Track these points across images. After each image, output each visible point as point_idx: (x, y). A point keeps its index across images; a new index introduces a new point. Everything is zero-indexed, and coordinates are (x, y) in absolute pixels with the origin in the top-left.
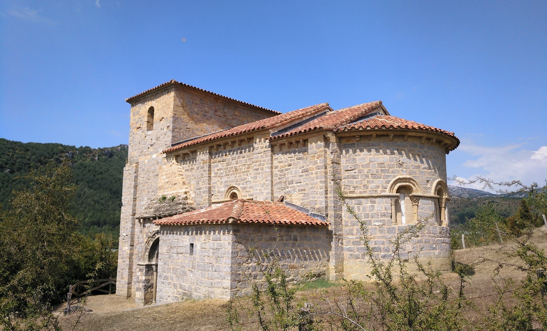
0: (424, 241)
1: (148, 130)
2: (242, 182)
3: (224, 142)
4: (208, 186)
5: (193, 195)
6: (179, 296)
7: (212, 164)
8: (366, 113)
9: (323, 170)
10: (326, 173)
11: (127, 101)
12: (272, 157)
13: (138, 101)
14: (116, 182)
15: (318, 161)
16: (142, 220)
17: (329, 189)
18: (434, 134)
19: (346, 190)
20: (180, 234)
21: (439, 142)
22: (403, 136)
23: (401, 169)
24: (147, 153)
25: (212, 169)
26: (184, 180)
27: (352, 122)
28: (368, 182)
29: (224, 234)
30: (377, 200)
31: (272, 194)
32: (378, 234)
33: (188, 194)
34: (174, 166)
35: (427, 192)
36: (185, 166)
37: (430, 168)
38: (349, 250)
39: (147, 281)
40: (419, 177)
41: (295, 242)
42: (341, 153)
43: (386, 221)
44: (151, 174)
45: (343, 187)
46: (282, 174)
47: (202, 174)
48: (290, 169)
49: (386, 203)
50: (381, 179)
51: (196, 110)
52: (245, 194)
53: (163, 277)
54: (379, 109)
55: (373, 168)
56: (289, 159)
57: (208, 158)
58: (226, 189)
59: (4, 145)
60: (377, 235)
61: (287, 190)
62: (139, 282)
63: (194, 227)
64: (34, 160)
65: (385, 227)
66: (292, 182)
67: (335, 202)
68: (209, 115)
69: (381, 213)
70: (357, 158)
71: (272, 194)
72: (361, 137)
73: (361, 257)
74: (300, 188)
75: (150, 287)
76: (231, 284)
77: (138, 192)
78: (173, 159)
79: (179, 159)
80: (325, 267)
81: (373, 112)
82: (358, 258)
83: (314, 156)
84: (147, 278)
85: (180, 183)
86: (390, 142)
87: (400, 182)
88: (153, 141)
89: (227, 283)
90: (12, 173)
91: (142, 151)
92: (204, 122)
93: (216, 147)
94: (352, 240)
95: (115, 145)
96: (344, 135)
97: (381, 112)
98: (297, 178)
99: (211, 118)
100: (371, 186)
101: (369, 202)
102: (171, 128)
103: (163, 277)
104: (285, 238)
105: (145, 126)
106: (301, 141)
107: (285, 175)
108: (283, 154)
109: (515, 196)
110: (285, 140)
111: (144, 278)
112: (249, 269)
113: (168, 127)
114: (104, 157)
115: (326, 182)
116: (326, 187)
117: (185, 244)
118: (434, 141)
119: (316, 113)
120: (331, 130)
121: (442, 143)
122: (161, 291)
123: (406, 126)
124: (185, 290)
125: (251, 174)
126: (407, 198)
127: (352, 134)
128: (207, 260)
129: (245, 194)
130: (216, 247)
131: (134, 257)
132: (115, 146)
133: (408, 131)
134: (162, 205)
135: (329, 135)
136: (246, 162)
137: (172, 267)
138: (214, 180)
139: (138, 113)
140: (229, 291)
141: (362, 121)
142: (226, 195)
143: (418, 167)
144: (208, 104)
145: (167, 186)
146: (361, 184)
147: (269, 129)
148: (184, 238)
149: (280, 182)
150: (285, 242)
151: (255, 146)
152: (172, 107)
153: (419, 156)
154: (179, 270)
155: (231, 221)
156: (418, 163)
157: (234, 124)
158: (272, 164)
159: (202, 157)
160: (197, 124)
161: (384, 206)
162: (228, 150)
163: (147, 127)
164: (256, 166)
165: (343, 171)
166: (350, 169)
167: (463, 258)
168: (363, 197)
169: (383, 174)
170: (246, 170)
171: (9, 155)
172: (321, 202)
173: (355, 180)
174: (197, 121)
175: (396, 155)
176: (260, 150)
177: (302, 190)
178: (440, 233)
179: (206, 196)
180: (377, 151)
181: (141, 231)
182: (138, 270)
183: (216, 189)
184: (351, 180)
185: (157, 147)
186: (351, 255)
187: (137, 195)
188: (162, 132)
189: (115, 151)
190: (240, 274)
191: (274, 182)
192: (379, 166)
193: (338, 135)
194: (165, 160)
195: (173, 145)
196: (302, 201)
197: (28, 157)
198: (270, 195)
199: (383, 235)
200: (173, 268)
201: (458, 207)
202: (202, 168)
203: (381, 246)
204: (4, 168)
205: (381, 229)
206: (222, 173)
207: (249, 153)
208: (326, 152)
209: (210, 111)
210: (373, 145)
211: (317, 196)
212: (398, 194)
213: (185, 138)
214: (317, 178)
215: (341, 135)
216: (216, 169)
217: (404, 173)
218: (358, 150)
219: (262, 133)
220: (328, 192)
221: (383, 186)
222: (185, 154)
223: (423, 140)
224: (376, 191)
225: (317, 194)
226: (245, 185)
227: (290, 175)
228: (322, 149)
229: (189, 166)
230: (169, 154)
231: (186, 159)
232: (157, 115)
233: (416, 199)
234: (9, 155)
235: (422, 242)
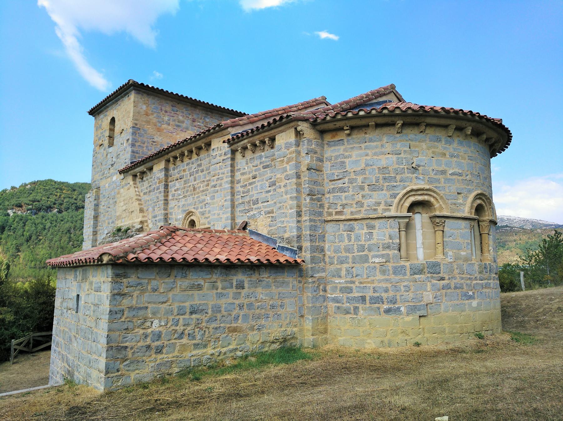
0: (453, 286)
1: (109, 147)
2: (201, 205)
4: (163, 212)
9: (294, 180)
10: (299, 184)
15: (288, 168)
17: (304, 209)
19: (330, 210)
22: (417, 125)
23: (415, 175)
24: (108, 175)
28: (363, 196)
30: (377, 223)
32: (379, 277)
33: (145, 224)
35: (458, 211)
38: (336, 300)
40: (444, 188)
41: (239, 291)
43: (391, 256)
45: (326, 206)
46: (246, 190)
47: (158, 198)
48: (254, 182)
49: (391, 227)
50: (384, 192)
56: (254, 168)
59: (52, 185)
60: (377, 278)
61: (252, 213)
64: (80, 200)
65: (390, 265)
66: (256, 202)
67: (313, 228)
68: (184, 125)
73: (352, 311)
74: (267, 209)
80: (296, 326)
82: (347, 312)
83: (283, 161)
85: (136, 210)
86: (398, 135)
88: (114, 160)
90: (60, 213)
94: (339, 286)
96: (325, 127)
98: (264, 195)
100: (366, 202)
101: (365, 228)
102: (130, 141)
104: (219, 284)
105: (106, 143)
106: (267, 140)
107: (248, 191)
110: (246, 141)
112: (146, 337)
118: (469, 132)
127: (339, 124)
133: (426, 116)
135: (303, 127)
136: (205, 178)
138: (172, 204)
144: (183, 113)
146: (353, 199)
147: (228, 128)
149: (243, 203)
150: (219, 290)
152: (131, 115)
155: (106, 259)
158: (232, 176)
161: (388, 231)
165: (326, 181)
166: (336, 178)
167: (521, 305)
168: (356, 220)
169: (388, 184)
170: (205, 188)
171: (56, 196)
172: (291, 228)
173: (344, 194)
183: (174, 216)
184: (339, 194)
186: (338, 308)
187: (98, 228)
190: (126, 347)
192: (381, 172)
197: (75, 197)
198: (230, 221)
199: (386, 277)
201: (520, 239)
203: (383, 294)
204: (52, 208)
205: (384, 268)
208: (299, 153)
209: (186, 121)
212: (410, 214)
216: (173, 189)
217: (419, 181)
219: (220, 133)
222: (143, 173)
224: (375, 210)
225: (286, 217)
226: (204, 209)
227: (255, 192)
231: (144, 179)
234: (56, 196)
235: (450, 288)
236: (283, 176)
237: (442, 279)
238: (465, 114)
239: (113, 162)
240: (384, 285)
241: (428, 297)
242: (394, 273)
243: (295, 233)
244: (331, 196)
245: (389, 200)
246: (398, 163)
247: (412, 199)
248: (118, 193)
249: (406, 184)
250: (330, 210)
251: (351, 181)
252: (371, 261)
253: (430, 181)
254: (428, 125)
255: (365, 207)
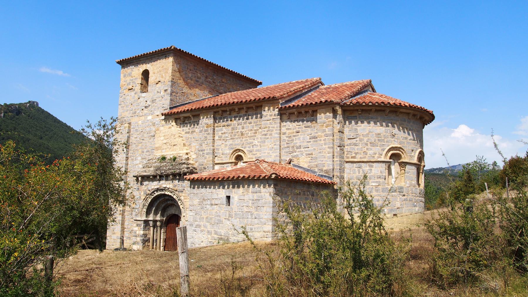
1: (142, 92)
3: (231, 108)
5: (194, 156)
6: (214, 241)
7: (216, 128)
8: (361, 90)
9: (332, 137)
11: (118, 63)
12: (280, 124)
13: (130, 63)
14: (24, 142)
15: (327, 130)
16: (140, 178)
17: (335, 154)
18: (419, 112)
19: (348, 156)
20: (214, 188)
21: (421, 118)
22: (396, 112)
23: (393, 139)
24: (141, 114)
25: (216, 132)
26: (184, 142)
27: (352, 97)
28: (367, 149)
29: (264, 187)
30: (374, 164)
31: (280, 157)
34: (173, 128)
35: (412, 160)
36: (185, 128)
37: (414, 140)
39: (145, 235)
42: (345, 124)
44: (145, 135)
45: (346, 153)
46: (290, 139)
47: (206, 137)
48: (298, 135)
49: (381, 167)
50: (378, 147)
51: (190, 75)
52: (252, 156)
53: (194, 226)
54: (368, 87)
55: (373, 137)
57: (212, 122)
58: (231, 151)
61: (295, 154)
62: (136, 236)
63: (231, 183)
65: (380, 187)
67: (341, 165)
68: (201, 81)
69: (377, 176)
70: (359, 128)
71: (280, 157)
72: (362, 110)
74: (307, 152)
75: (147, 241)
76: (272, 228)
77: (130, 152)
78: (172, 122)
79: (178, 121)
81: (365, 89)
83: (323, 126)
84: (145, 232)
85: (180, 144)
86: (386, 117)
87: (393, 150)
88: (148, 103)
89: (269, 227)
91: (135, 113)
92: (196, 88)
93: (221, 112)
95: (23, 102)
96: (348, 108)
97: (371, 89)
98: (305, 144)
99: (203, 83)
100: (370, 152)
102: (169, 91)
103: (194, 226)
105: (138, 88)
106: (310, 111)
107: (293, 140)
108: (291, 122)
109: (435, 172)
111: (142, 232)
113: (166, 90)
114: (10, 114)
115: (333, 148)
116: (333, 152)
117: (220, 196)
119: (312, 86)
120: (338, 104)
121: (417, 118)
122: (193, 237)
123: (400, 104)
124: (221, 235)
125: (257, 138)
126: (397, 164)
127: (356, 108)
128: (245, 209)
129: (252, 156)
130: (255, 198)
131: (126, 214)
132: (23, 102)
133: (401, 108)
134: (162, 164)
135: (338, 108)
136: (253, 128)
137: (205, 217)
138: (217, 143)
139: (130, 75)
140: (270, 235)
141: (358, 96)
142: (230, 157)
143: (406, 138)
145: (165, 146)
146: (362, 150)
148: (219, 191)
151: (264, 113)
152: (170, 71)
153: (407, 129)
154: (213, 219)
155: (273, 176)
156: (406, 135)
157: (221, 91)
158: (280, 130)
159: (206, 121)
160: (190, 89)
161: (380, 169)
162: (233, 116)
163: (141, 89)
164: (264, 131)
165: (346, 139)
170: (252, 135)
172: (329, 165)
174: (191, 87)
175: (390, 128)
176: (268, 117)
177: (309, 154)
178: (420, 193)
179: (210, 157)
180: (375, 123)
181: (138, 189)
182: (135, 225)
183: (220, 151)
185: (153, 109)
187: (129, 155)
188: (159, 95)
189: (23, 108)
191: (282, 147)
193: (344, 108)
194: (163, 122)
195: (171, 108)
196: (309, 164)
198: (279, 158)
199: (378, 193)
200: (207, 218)
202: (206, 131)
206: (227, 137)
207: (256, 120)
210: (372, 118)
211: (324, 159)
212: (391, 160)
213: (181, 102)
214: (325, 144)
215: (346, 108)
216: (220, 133)
218: (359, 122)
220: (335, 156)
221: (379, 153)
223: (411, 116)
224: (373, 157)
226: (251, 148)
227: (297, 141)
228: (331, 119)
229: (189, 129)
230: (168, 117)
231: (186, 122)
232: (151, 79)
233: (403, 165)
236: (323, 134)
237: (404, 195)
238: (418, 108)
239: (147, 105)
240: (377, 198)
241: (398, 204)
242: (382, 191)
243: (331, 167)
244: (349, 147)
245: (381, 152)
246: (386, 132)
247: (391, 152)
248: (158, 130)
249: (389, 144)
250: (348, 156)
251: (361, 140)
252: (370, 184)
253: (400, 144)
254: (401, 113)
255: (368, 155)
